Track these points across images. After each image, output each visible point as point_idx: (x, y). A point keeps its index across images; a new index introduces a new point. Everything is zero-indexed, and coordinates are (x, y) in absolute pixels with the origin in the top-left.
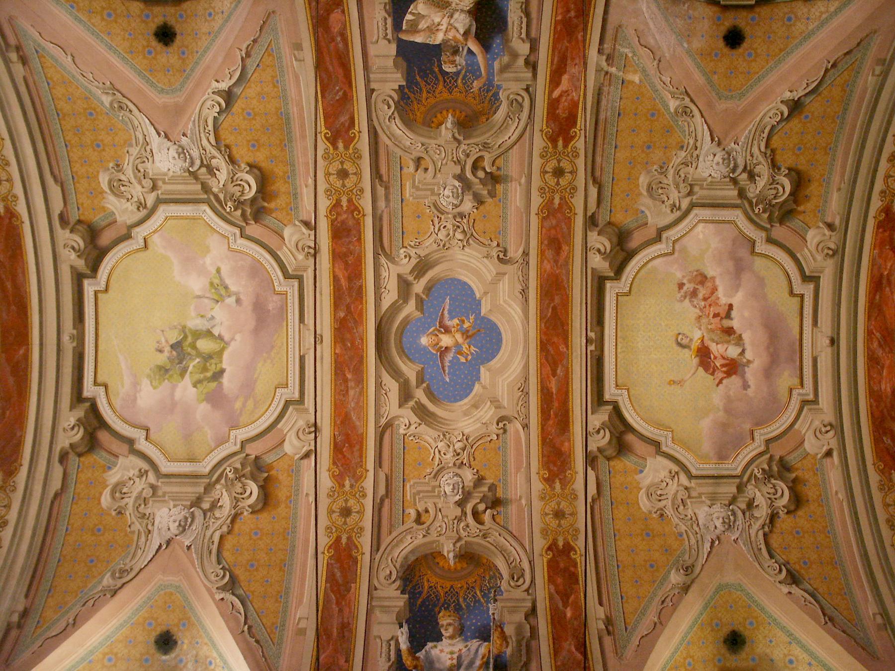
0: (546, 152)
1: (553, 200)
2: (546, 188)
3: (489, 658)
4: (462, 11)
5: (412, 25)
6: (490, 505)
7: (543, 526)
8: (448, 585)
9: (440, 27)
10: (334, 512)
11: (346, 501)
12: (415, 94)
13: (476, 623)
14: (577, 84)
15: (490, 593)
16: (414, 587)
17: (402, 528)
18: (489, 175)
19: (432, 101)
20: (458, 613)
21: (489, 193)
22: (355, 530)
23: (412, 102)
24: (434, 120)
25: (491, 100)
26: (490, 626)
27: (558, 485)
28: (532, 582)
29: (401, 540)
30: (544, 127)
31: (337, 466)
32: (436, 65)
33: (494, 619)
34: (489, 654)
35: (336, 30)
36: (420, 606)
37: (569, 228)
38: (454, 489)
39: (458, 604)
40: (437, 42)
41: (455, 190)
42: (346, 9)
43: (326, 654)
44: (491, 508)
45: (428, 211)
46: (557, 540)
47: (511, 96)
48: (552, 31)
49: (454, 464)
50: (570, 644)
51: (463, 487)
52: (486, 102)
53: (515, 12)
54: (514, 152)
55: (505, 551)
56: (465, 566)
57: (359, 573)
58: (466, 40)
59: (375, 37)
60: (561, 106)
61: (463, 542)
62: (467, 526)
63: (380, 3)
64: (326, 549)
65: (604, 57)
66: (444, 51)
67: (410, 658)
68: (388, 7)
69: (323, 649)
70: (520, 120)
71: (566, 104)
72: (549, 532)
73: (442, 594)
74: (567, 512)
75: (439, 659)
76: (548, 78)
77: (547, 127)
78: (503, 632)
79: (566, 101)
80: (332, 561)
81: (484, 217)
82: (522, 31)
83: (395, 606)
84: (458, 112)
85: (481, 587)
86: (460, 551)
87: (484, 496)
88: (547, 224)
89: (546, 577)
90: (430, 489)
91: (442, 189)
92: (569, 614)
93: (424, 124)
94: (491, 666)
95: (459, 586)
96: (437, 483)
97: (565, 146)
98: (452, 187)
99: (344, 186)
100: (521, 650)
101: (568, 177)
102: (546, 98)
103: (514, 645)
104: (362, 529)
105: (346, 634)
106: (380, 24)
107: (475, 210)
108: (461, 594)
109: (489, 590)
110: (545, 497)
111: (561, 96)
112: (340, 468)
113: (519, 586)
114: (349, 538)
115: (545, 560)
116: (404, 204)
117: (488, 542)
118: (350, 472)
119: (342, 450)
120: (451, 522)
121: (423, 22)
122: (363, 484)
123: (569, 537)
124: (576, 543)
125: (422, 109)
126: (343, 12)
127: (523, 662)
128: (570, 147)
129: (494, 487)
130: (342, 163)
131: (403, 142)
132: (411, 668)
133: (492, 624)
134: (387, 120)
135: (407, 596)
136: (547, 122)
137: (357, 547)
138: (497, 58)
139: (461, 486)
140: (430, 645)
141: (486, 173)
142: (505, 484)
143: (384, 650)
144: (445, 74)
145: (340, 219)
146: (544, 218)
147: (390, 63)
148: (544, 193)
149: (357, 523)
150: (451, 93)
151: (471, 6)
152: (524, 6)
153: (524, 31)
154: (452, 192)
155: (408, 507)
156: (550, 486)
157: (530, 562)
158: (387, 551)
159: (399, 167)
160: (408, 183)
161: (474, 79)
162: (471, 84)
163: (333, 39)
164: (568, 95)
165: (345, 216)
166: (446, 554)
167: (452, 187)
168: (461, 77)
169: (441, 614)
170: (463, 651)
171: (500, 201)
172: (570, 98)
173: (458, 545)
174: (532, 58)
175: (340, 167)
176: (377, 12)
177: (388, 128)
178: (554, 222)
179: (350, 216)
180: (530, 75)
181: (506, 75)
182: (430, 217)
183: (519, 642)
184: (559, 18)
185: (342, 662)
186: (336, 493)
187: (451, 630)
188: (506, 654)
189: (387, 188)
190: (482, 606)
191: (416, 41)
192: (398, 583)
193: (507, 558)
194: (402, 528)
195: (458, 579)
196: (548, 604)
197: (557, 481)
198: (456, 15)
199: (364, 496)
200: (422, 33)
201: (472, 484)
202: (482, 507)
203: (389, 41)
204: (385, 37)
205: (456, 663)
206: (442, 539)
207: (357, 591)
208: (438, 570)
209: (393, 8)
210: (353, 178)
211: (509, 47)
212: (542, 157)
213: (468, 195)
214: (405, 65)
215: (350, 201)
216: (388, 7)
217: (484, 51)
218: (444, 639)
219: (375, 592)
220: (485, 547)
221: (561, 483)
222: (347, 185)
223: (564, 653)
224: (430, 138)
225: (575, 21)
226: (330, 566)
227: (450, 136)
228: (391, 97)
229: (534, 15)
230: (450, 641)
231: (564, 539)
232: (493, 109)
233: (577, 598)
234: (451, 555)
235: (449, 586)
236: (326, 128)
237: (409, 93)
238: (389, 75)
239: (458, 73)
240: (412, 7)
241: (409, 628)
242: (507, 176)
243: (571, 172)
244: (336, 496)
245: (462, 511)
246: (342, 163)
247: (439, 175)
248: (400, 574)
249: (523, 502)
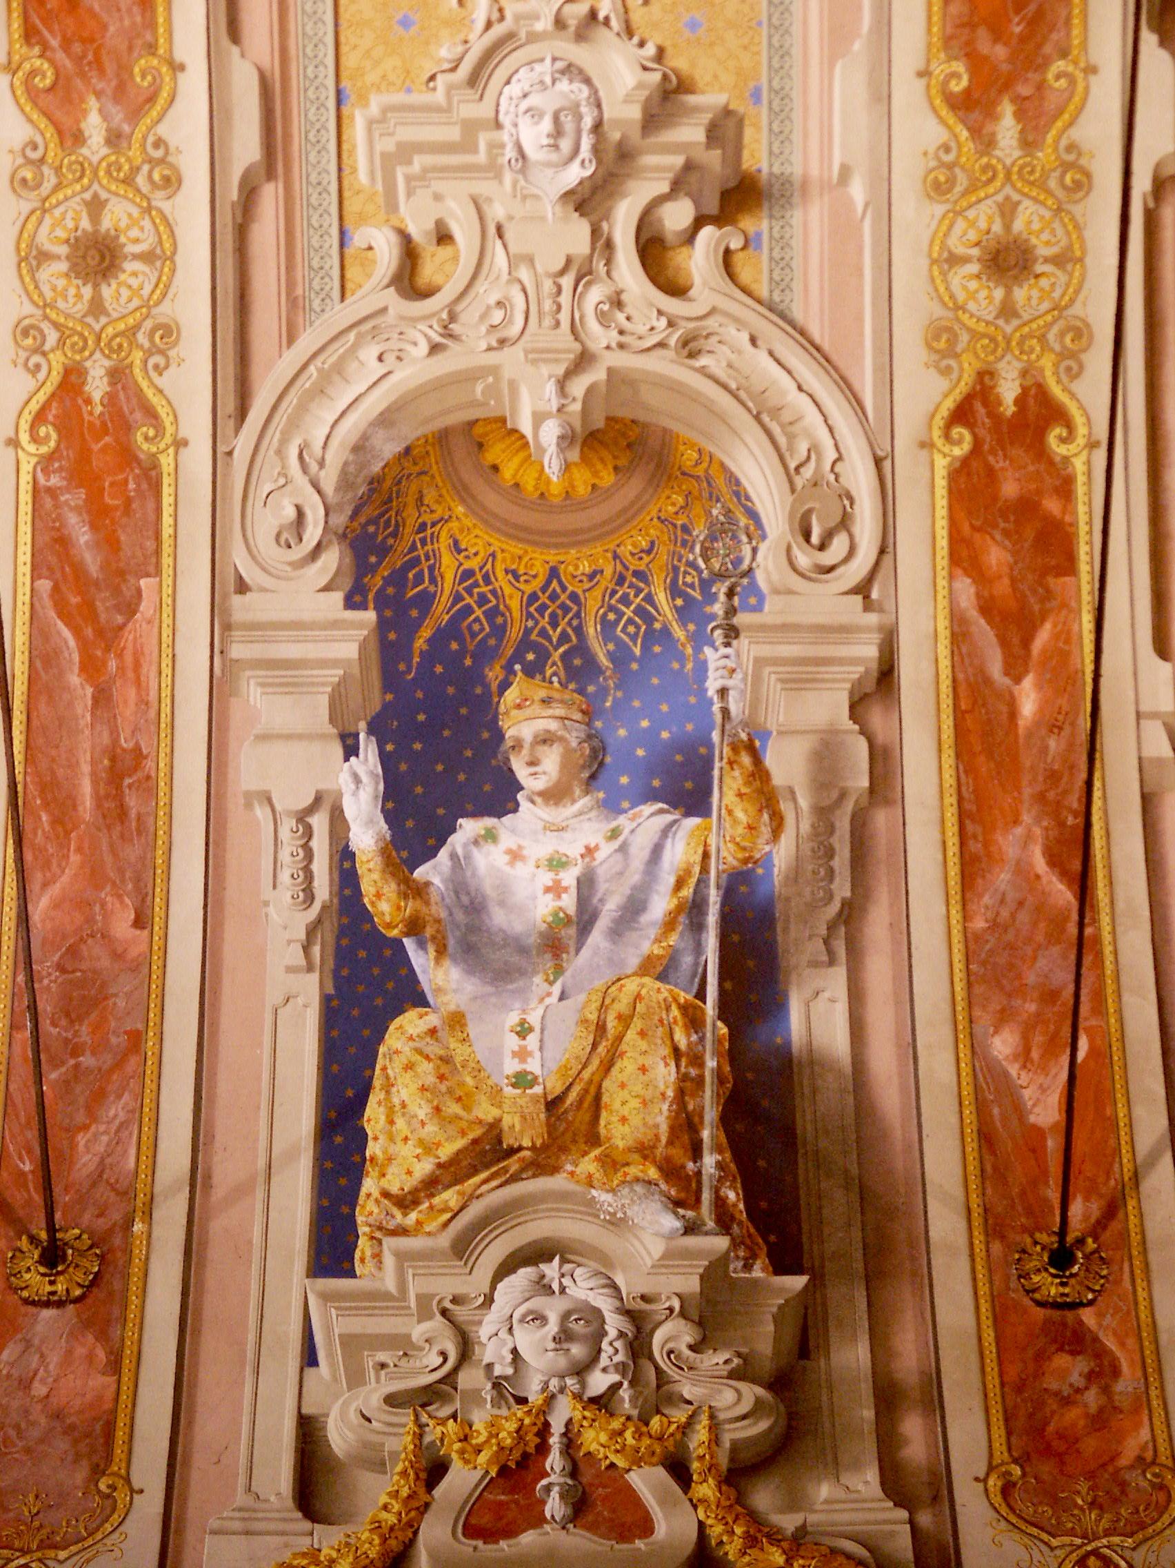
3: (702, 882)
6: (713, 207)
7: (939, 311)
8: (538, 562)
10: (44, 257)
11: (96, 207)
13: (653, 731)
15: (711, 598)
16: (398, 578)
17: (341, 315)
20: (581, 691)
22: (141, 338)
26: (709, 745)
27: (1007, 127)
28: (882, 551)
29: (339, 369)
31: (45, 47)
33: (725, 712)
34: (705, 869)
36: (429, 658)
38: (558, 132)
39: (582, 648)
43: (55, 890)
44: (721, 219)
46: (991, 374)
49: (560, 23)
50: (1028, 838)
51: (597, 127)
55: (776, 412)
56: (607, 478)
57: (167, 531)
61: (596, 375)
62: (618, 303)
64: (24, 426)
67: (391, 889)
69: (47, 865)
72: (964, 338)
73: (515, 604)
74: (1043, 251)
75: (504, 888)
78: (759, 773)
80: (55, 481)
83: (324, 663)
85: (676, 569)
86: (585, 411)
87: (689, 167)
89: (943, 542)
90: (453, 134)
92: (1029, 701)
94: (712, 918)
95: (585, 567)
96: (484, 110)
100: (830, 853)
103: (805, 827)
104: (169, 331)
105: (132, 802)
108: (593, 604)
109: (705, 585)
110: (951, 182)
112: (60, 56)
113: (831, 569)
114: (117, 375)
115: (941, 464)
117: (703, 371)
118: (101, 71)
119: (122, 778)
120: (548, 285)
122: (162, 130)
123: (1047, 363)
124: (1076, 387)
127: (836, 906)
129: (731, 123)
132: (394, 933)
133: (715, 736)
135: (370, 616)
137: (151, 414)
139: (588, 122)
140: (468, 828)
142: (780, 114)
143: (285, 856)
149: (146, 304)
155: (363, 219)
156: (975, 132)
157: (878, 462)
158: (280, 419)
166: (526, 428)
169: (511, 695)
170: (600, 855)
173: (578, 387)
183: (824, 813)
185: (122, 926)
186: (46, 170)
187: (551, 761)
188: (769, 873)
190: (682, 658)
192: (332, 559)
193: (782, 441)
194: (341, 315)
195: (576, 538)
196: (945, 663)
197: (1007, 110)
199: (172, 182)
201: (634, 113)
202: (677, 216)
205: (571, 909)
206: (511, 361)
207: (167, 610)
208: (491, 500)
218: (524, 805)
219: (237, 600)
220: (694, 397)
221: (1020, 115)
223: (1003, 878)
226: (48, 502)
230: (545, 813)
231: (1024, 373)
233: (1066, 636)
234: (550, 433)
235: (541, 571)
241: (384, 757)
244: (47, 186)
245: (595, 232)
248: (340, 520)
249: (857, 191)
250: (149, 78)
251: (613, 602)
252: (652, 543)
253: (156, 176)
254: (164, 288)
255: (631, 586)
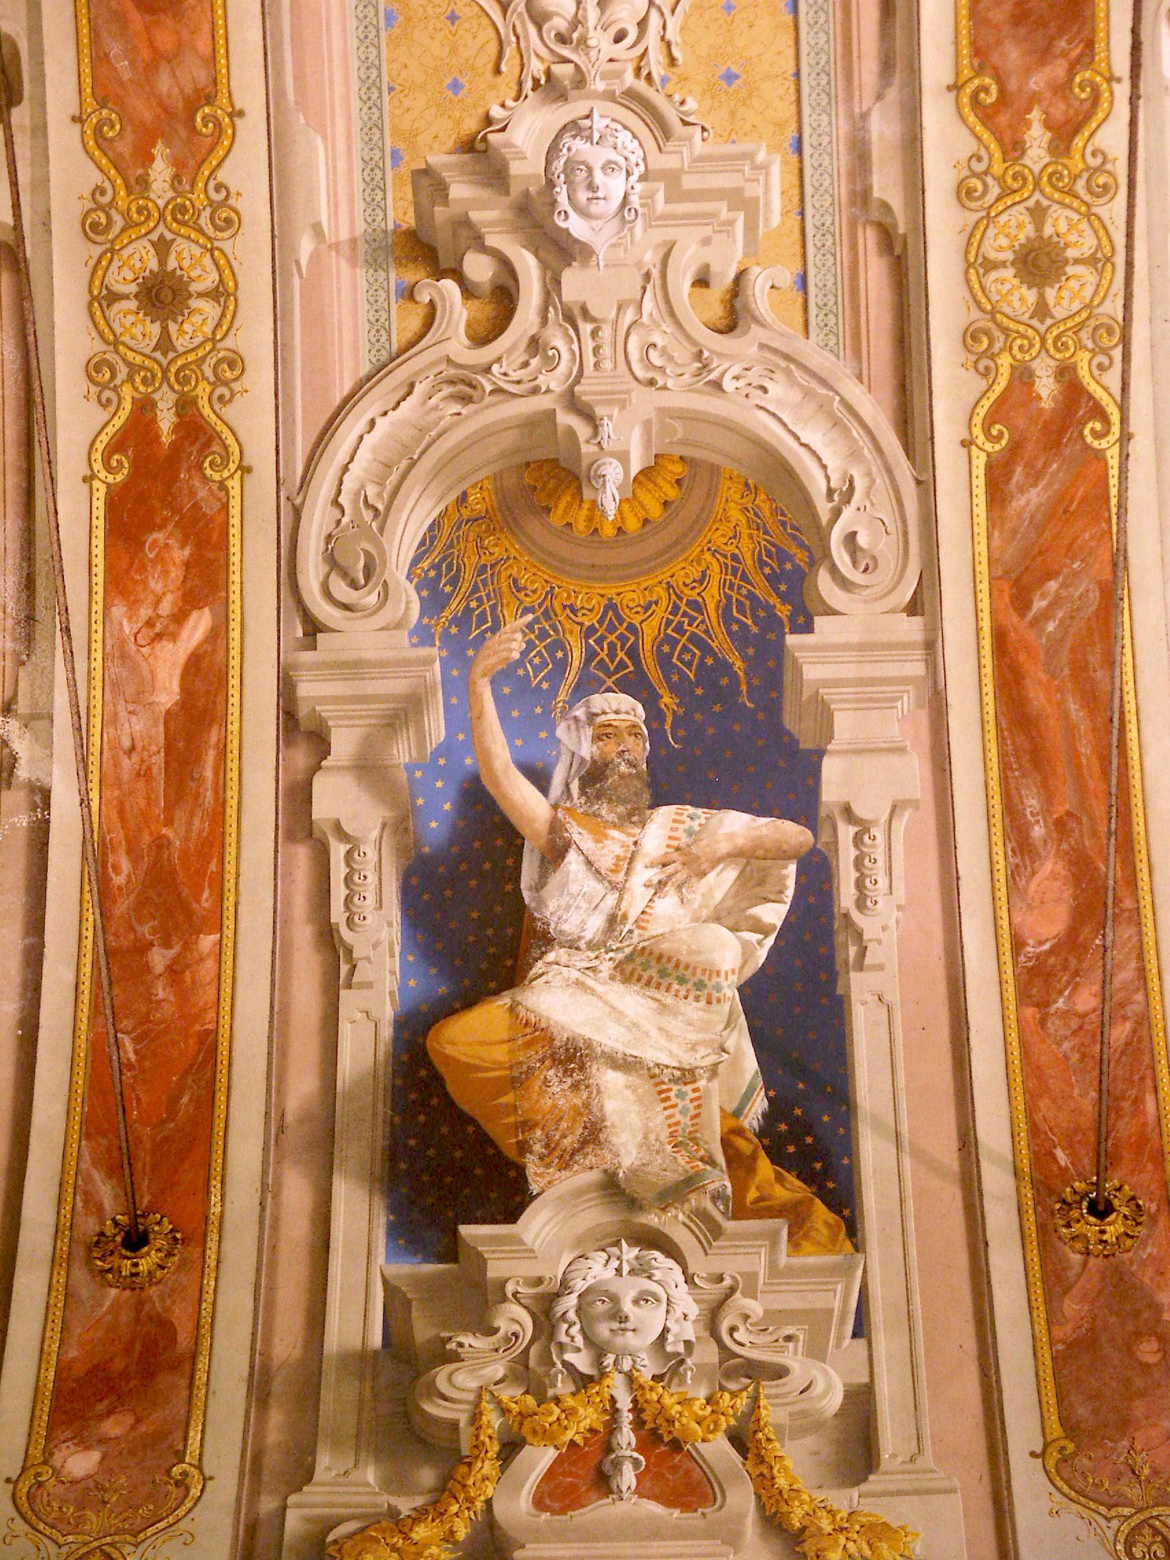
0: (220, 381)
1: (176, 178)
2: (210, 231)
4: (573, 945)
5: (761, 883)
9: (655, 875)
12: (751, 596)
14: (116, 669)
18: (445, 262)
19: (682, 572)
21: (440, 189)
23: (762, 564)
24: (672, 493)
25: (454, 581)
30: (234, 484)
32: (669, 720)
35: (1048, 866)
37: (100, 59)
40: (664, 814)
41: (582, 195)
42: (1007, 958)
45: (691, 104)
47: (372, 599)
48: (230, 884)
52: (468, 575)
53: (375, 946)
54: (348, 364)
58: (555, 827)
59: (900, 826)
60: (176, 574)
63: (880, 967)
65: (22, 773)
66: (638, 776)
68: (853, 950)
70: (336, 503)
71: (156, 585)
76: (234, 692)
77: (222, 485)
79: (158, 602)
81: (456, 86)
82: (344, 892)
84: (581, 525)
88: (193, 74)
91: (635, 200)
93: (715, 470)
97: (145, 407)
98: (594, 209)
99: (1038, 214)
101: (122, 280)
102: (235, 607)
106: (883, 882)
107: (496, 112)
111: (180, 617)
116: (791, 132)
121: (719, 895)
125: (719, 538)
126: (1018, 944)
128: (127, 405)
130: (1042, 310)
131: (795, 396)
134: (859, 484)
136: (225, 507)
138: (437, 753)
141: (457, 275)
144: (635, 685)
145: (1058, 69)
146: (210, 100)
147: (845, 725)
148: (215, 206)
150: (611, 606)
151: (539, 967)
152: (344, 969)
153: (338, 870)
154: (591, 187)
159: (812, 290)
160: (776, 219)
161: (520, 663)
162: (530, 645)
163: (1061, 826)
164: (150, 623)
165: (1037, 82)
167: (594, 209)
168: (572, 676)
171: (396, 156)
172: (145, 613)
174: (300, 757)
175: (1050, 293)
176: (893, 936)
177: (854, 455)
178: (164, 83)
179: (1013, 85)
180: (306, 689)
181: (397, 686)
182: (684, 79)
184: (207, 942)
189: (862, 197)
191: (746, 817)
195: (628, 572)
198: (594, 925)
199: (230, 223)
200: (724, 847)
203: (847, 811)
204: (863, 828)
209: (832, 947)
210: (998, 245)
211: (393, 803)
212: (235, 361)
213: (528, 177)
214: (789, 722)
215: (1014, 148)
216: (853, 950)
217: (485, 781)
222: (1026, 218)
224: (691, 417)
225: (146, 930)
227: (607, 428)
228: (844, 584)
229: (303, 935)
232: (439, 546)
236: (1099, 456)
237: (774, 600)
238: (850, 671)
239: (584, 688)
240: (762, 955)
242: (373, 263)
243: (114, 297)
246: (1042, 310)
247: (650, 258)
250: (211, 125)
251: (669, 631)
252: (704, 573)
253: (985, 341)
254: (971, 238)
255: (685, 614)
